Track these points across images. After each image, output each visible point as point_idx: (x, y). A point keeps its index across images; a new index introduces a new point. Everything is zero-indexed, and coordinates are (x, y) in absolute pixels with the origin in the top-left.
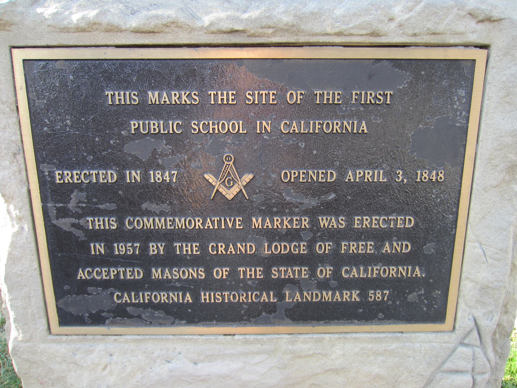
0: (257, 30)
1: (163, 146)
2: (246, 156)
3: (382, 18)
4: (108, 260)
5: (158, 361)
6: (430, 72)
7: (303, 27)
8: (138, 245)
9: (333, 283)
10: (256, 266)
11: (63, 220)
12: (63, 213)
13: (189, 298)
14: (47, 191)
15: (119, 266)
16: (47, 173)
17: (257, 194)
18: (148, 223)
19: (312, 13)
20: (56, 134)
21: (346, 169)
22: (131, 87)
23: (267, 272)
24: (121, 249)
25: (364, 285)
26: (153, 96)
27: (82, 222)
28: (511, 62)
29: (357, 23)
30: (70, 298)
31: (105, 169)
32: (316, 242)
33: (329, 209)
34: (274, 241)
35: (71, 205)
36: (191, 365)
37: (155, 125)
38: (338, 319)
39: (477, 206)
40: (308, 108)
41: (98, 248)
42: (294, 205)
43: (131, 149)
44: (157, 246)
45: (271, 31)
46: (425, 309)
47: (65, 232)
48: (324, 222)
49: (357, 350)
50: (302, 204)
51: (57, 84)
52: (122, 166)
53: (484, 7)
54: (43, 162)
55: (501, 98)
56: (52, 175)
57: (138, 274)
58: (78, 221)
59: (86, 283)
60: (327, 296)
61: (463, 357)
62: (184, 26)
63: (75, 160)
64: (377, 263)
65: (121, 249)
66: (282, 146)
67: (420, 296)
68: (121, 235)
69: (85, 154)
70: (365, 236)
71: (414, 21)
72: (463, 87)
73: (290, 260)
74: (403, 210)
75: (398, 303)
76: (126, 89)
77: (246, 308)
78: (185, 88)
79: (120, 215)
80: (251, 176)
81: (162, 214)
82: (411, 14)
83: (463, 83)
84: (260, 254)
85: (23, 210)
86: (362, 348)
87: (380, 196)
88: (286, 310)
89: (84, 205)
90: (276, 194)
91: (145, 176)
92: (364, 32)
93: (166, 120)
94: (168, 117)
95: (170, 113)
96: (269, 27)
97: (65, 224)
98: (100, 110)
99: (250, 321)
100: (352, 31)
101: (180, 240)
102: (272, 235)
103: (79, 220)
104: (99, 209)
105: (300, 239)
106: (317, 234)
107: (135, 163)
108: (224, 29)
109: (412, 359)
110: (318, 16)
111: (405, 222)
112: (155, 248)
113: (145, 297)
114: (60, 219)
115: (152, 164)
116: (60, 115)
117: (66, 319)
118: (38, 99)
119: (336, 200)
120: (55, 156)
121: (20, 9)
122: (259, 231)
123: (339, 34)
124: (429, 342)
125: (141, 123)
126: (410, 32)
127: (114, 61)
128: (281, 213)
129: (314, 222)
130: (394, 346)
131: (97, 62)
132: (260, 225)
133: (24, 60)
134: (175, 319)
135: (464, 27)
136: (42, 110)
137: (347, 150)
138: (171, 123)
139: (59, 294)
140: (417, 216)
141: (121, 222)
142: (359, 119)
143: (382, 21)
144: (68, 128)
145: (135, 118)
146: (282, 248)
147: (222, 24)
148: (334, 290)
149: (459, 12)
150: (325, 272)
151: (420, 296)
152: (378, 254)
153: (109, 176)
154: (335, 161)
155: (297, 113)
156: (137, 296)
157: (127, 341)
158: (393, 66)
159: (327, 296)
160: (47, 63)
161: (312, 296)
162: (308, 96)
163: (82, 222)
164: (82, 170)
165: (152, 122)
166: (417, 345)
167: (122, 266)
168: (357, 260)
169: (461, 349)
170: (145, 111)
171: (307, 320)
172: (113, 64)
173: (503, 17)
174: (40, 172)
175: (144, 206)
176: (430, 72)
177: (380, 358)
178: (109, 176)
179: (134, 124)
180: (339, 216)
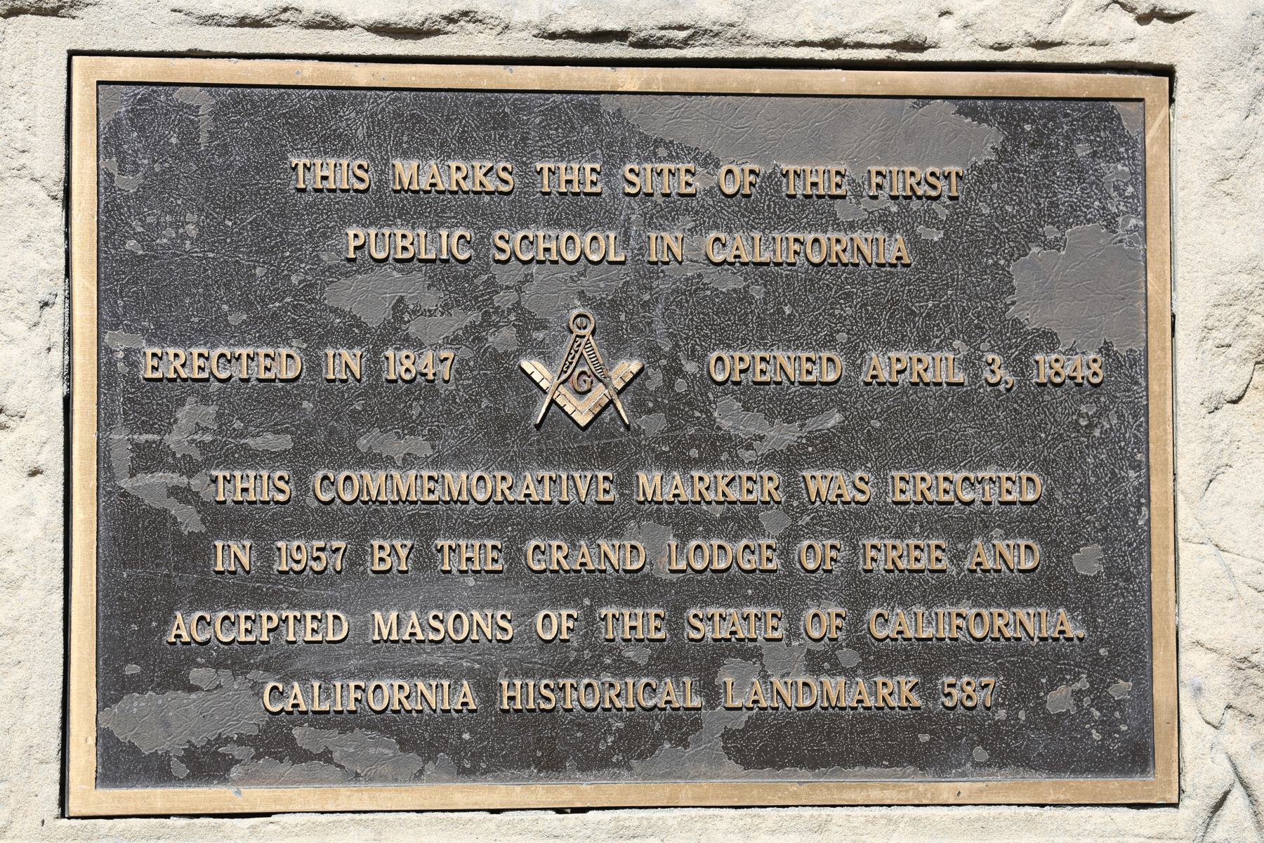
0: (653, 32)
1: (415, 288)
2: (623, 318)
3: (924, 10)
4: (259, 589)
6: (1045, 125)
9: (849, 657)
11: (144, 479)
12: (148, 458)
13: (467, 694)
14: (113, 401)
15: (285, 605)
16: (121, 355)
17: (650, 412)
18: (374, 482)
20: (156, 258)
21: (865, 351)
22: (352, 149)
23: (675, 621)
24: (293, 553)
25: (930, 660)
26: (406, 170)
27: (196, 483)
28: (1221, 104)
29: (871, 20)
30: (136, 703)
31: (272, 346)
33: (827, 450)
34: (694, 536)
35: (175, 440)
38: (867, 763)
39: (1192, 446)
40: (769, 206)
41: (231, 554)
42: (741, 442)
45: (683, 35)
46: (1096, 736)
47: (149, 511)
48: (824, 483)
50: (761, 438)
51: (174, 140)
52: (317, 337)
54: (115, 327)
55: (1213, 185)
58: (186, 481)
59: (192, 652)
60: (837, 690)
62: (487, 21)
63: (199, 323)
64: (959, 600)
65: (293, 553)
66: (708, 293)
67: (1078, 695)
68: (296, 518)
69: (225, 307)
70: (921, 526)
72: (1123, 158)
73: (726, 586)
74: (1013, 456)
75: (1022, 715)
76: (339, 153)
77: (618, 730)
79: (300, 461)
80: (635, 366)
81: (409, 461)
83: (1122, 150)
84: (658, 571)
85: (47, 448)
87: (952, 420)
88: (728, 735)
89: (208, 438)
90: (697, 414)
91: (375, 362)
92: (887, 39)
93: (431, 228)
94: (437, 221)
95: (443, 211)
96: (681, 28)
97: (151, 485)
98: (272, 202)
99: (630, 769)
101: (452, 532)
102: (686, 520)
103: (190, 477)
104: (245, 447)
105: (756, 529)
106: (805, 517)
107: (351, 332)
114: (139, 476)
115: (394, 332)
116: (171, 213)
117: (120, 763)
119: (843, 430)
120: (148, 311)
126: (990, 41)
127: (1027, 104)
128: (710, 461)
129: (792, 486)
132: (658, 492)
133: (99, 83)
134: (425, 761)
135: (1106, 29)
136: (127, 198)
137: (864, 305)
138: (444, 233)
139: (112, 687)
140: (1048, 474)
142: (889, 231)
144: (188, 242)
145: (358, 222)
146: (711, 554)
148: (850, 673)
150: (823, 621)
151: (1078, 695)
152: (958, 574)
153: (286, 363)
154: (839, 331)
155: (744, 216)
156: (327, 692)
159: (837, 690)
160: (154, 92)
161: (797, 691)
162: (770, 176)
163: (196, 483)
164: (214, 346)
172: (313, 99)
173: (1190, 9)
174: (103, 349)
175: (363, 443)
176: (1045, 125)
179: (354, 234)
180: (854, 469)
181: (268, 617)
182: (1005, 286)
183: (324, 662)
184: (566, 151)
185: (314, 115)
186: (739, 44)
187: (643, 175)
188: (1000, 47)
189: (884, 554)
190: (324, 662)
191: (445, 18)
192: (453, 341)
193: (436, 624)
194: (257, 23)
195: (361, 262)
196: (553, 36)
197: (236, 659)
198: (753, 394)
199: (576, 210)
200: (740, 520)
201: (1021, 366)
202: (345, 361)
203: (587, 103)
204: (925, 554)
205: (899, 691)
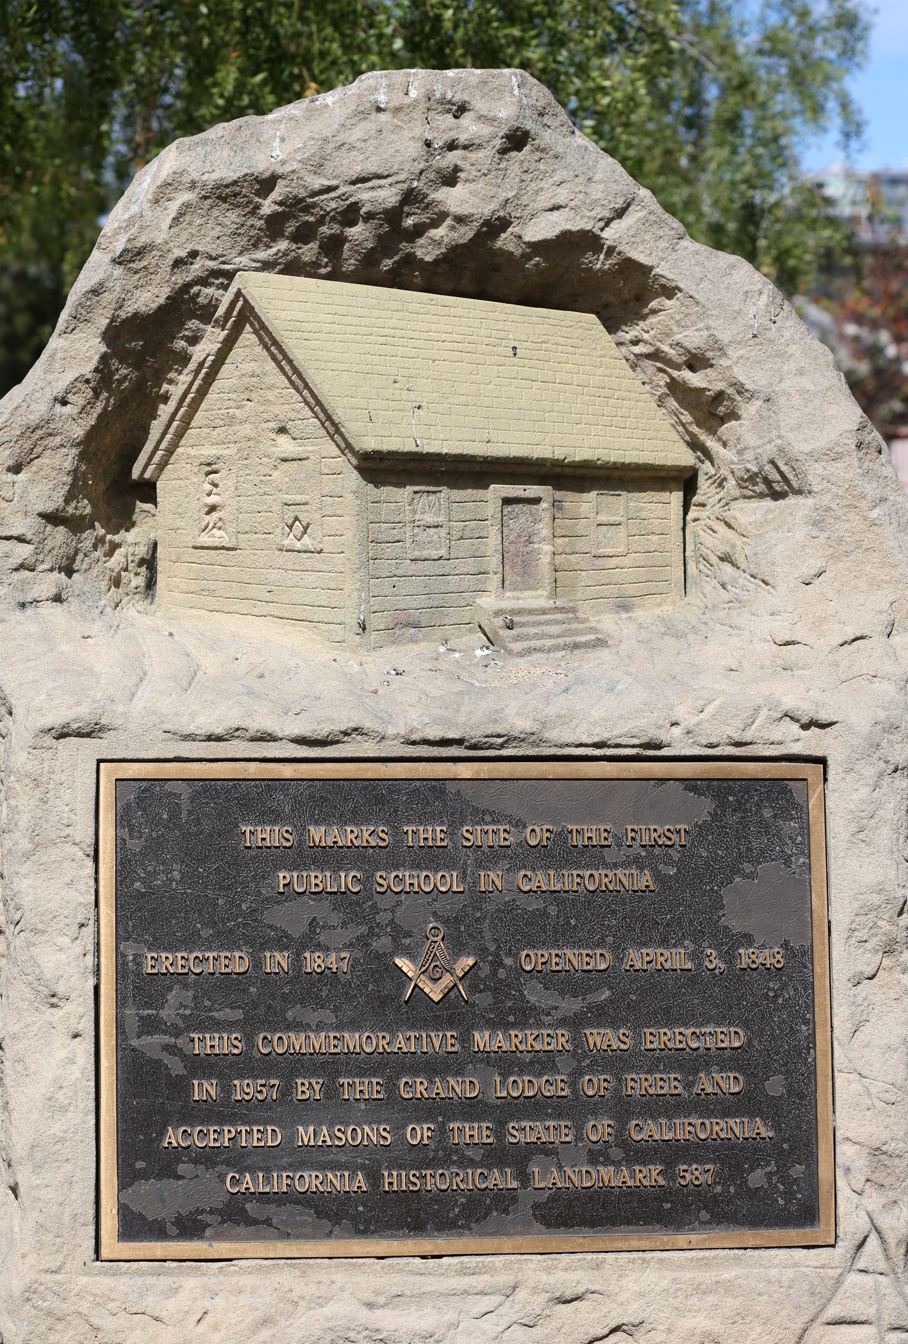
2: (463, 929)
5: (303, 1303)
6: (742, 797)
7: (547, 735)
8: (277, 1082)
9: (616, 1153)
10: (479, 1119)
11: (147, 1040)
12: (149, 1026)
13: (361, 1181)
16: (131, 958)
17: (481, 991)
18: (297, 1041)
19: (559, 717)
24: (245, 1089)
25: (671, 1154)
26: (318, 834)
27: (180, 1042)
30: (144, 1187)
32: (582, 1074)
33: (600, 1016)
35: (167, 1013)
36: (365, 1311)
37: (318, 879)
38: (628, 1223)
41: (205, 1089)
43: (279, 917)
44: (310, 1083)
45: (500, 740)
48: (599, 1038)
49: (664, 1284)
50: (556, 1008)
51: (165, 817)
52: (259, 944)
53: (805, 707)
56: (138, 960)
57: (272, 1136)
61: (859, 1292)
65: (245, 1089)
67: (769, 1175)
71: (707, 725)
73: (534, 1108)
76: (273, 822)
77: (462, 1204)
78: (367, 821)
80: (471, 961)
81: (320, 1027)
82: (702, 716)
86: (675, 1279)
87: (684, 994)
88: (536, 1206)
91: (297, 961)
96: (499, 736)
99: (470, 1229)
100: (619, 741)
102: (507, 1064)
103: (176, 1038)
106: (583, 1060)
107: (282, 942)
108: (431, 738)
109: (766, 1297)
110: (568, 720)
111: (731, 1038)
112: (308, 1088)
113: (280, 1183)
115: (310, 941)
116: (163, 864)
117: (134, 1226)
118: (131, 837)
119: (612, 1002)
121: (120, 708)
122: (451, 864)
123: (597, 745)
124: (795, 1265)
125: (295, 874)
128: (521, 1024)
129: (577, 1040)
130: (727, 1275)
131: (231, 783)
134: (333, 1225)
141: (249, 1040)
143: (659, 727)
146: (523, 1086)
147: (427, 730)
148: (617, 1164)
149: (771, 713)
150: (600, 1129)
153: (238, 962)
156: (268, 1180)
157: (243, 1272)
158: (685, 789)
161: (581, 1177)
163: (180, 1042)
164: (191, 952)
165: (313, 875)
166: (774, 1272)
167: (244, 1123)
168: (655, 1107)
169: (854, 1278)
170: (305, 856)
171: (572, 1227)
174: (119, 955)
176: (742, 797)
177: (711, 1299)
178: (238, 962)
179: (283, 877)
184: (425, 818)
186: (538, 746)
187: (474, 834)
191: (342, 732)
192: (349, 946)
193: (339, 1134)
194: (219, 739)
195: (288, 895)
196: (414, 743)
197: (208, 1158)
198: (549, 978)
199: (430, 858)
200: (543, 1063)
201: (729, 957)
202: (277, 961)
203: (437, 786)
205: (650, 1175)
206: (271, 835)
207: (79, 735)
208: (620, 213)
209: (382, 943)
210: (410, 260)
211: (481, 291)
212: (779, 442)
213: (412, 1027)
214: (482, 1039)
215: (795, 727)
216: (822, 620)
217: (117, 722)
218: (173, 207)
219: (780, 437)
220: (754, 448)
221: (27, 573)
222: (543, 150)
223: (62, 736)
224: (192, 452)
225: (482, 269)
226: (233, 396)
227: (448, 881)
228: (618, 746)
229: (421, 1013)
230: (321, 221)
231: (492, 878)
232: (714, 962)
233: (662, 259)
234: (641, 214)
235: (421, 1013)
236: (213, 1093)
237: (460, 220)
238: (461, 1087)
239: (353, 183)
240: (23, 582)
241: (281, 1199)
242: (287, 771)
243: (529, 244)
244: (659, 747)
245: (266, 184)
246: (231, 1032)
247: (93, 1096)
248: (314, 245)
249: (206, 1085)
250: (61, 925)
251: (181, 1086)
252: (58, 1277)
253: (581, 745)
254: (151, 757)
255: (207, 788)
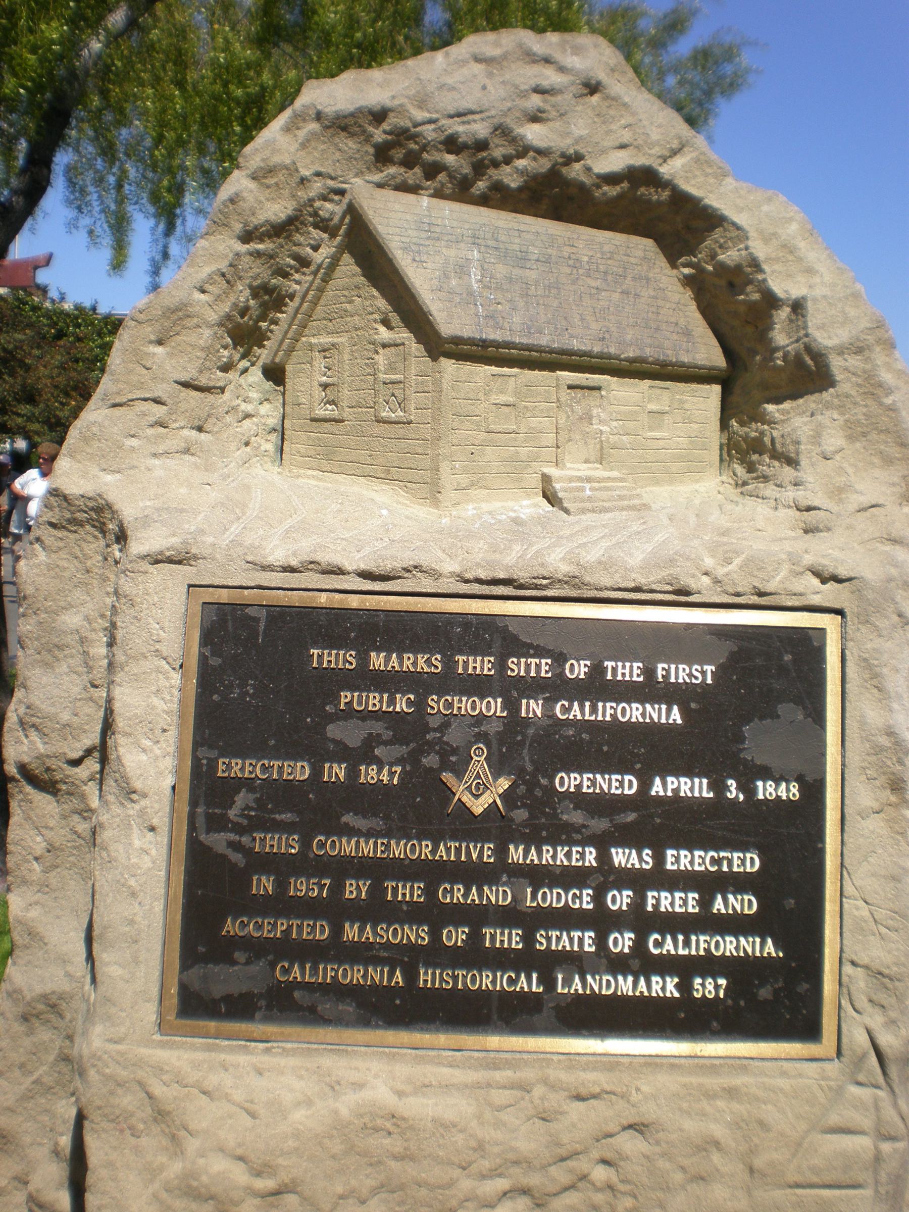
4: (282, 905)
12: (217, 823)
18: (348, 847)
24: (302, 887)
25: (686, 969)
26: (377, 660)
27: (245, 840)
37: (375, 701)
41: (264, 884)
45: (545, 582)
48: (621, 857)
52: (318, 755)
54: (202, 745)
56: (213, 765)
57: (322, 932)
59: (236, 942)
60: (625, 985)
65: (302, 887)
68: (306, 865)
81: (369, 834)
82: (730, 567)
91: (353, 773)
92: (669, 588)
96: (544, 578)
97: (218, 841)
102: (539, 876)
103: (241, 836)
104: (274, 819)
106: (607, 877)
107: (343, 753)
111: (747, 862)
112: (355, 889)
113: (328, 972)
115: (367, 754)
121: (210, 540)
126: (731, 591)
129: (604, 857)
150: (622, 942)
153: (301, 771)
156: (315, 971)
159: (625, 985)
164: (259, 760)
178: (301, 771)
179: (345, 697)
181: (282, 925)
182: (741, 739)
183: (313, 953)
184: (474, 651)
185: (336, 626)
186: (579, 588)
187: (517, 667)
188: (738, 595)
189: (666, 901)
190: (313, 953)
191: (404, 569)
192: (400, 761)
193: (382, 933)
194: (292, 570)
195: (349, 713)
196: (467, 581)
197: (258, 949)
198: (578, 798)
199: (478, 686)
200: (572, 878)
201: (747, 788)
202: (337, 771)
203: (488, 622)
204: (684, 902)
205: (665, 987)
206: (342, 659)
207: (170, 561)
208: (674, 153)
209: (430, 760)
210: (498, 187)
211: (557, 214)
212: (806, 340)
213: (454, 838)
214: (516, 854)
215: (816, 582)
216: (840, 490)
217: (206, 552)
218: (302, 134)
219: (807, 335)
220: (784, 347)
221: (161, 430)
222: (613, 99)
223: (157, 562)
224: (313, 340)
225: (556, 195)
226: (346, 293)
227: (494, 707)
228: (652, 591)
229: (468, 826)
230: (424, 148)
231: (533, 708)
232: (733, 791)
233: (710, 192)
234: (694, 155)
235: (468, 826)
236: (270, 889)
237: (540, 152)
238: (498, 895)
239: (451, 117)
240: (157, 437)
241: (324, 988)
242: (354, 602)
243: (599, 176)
244: (688, 593)
245: (379, 116)
246: (290, 834)
247: (847, 715)
248: (417, 170)
249: (264, 879)
250: (146, 730)
251: (242, 878)
252: (120, 1047)
253: (620, 589)
254: (235, 584)
255: (280, 615)
